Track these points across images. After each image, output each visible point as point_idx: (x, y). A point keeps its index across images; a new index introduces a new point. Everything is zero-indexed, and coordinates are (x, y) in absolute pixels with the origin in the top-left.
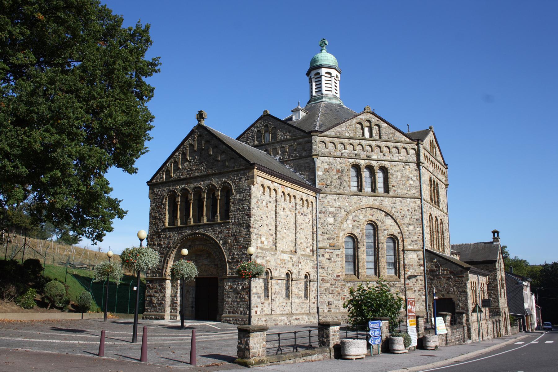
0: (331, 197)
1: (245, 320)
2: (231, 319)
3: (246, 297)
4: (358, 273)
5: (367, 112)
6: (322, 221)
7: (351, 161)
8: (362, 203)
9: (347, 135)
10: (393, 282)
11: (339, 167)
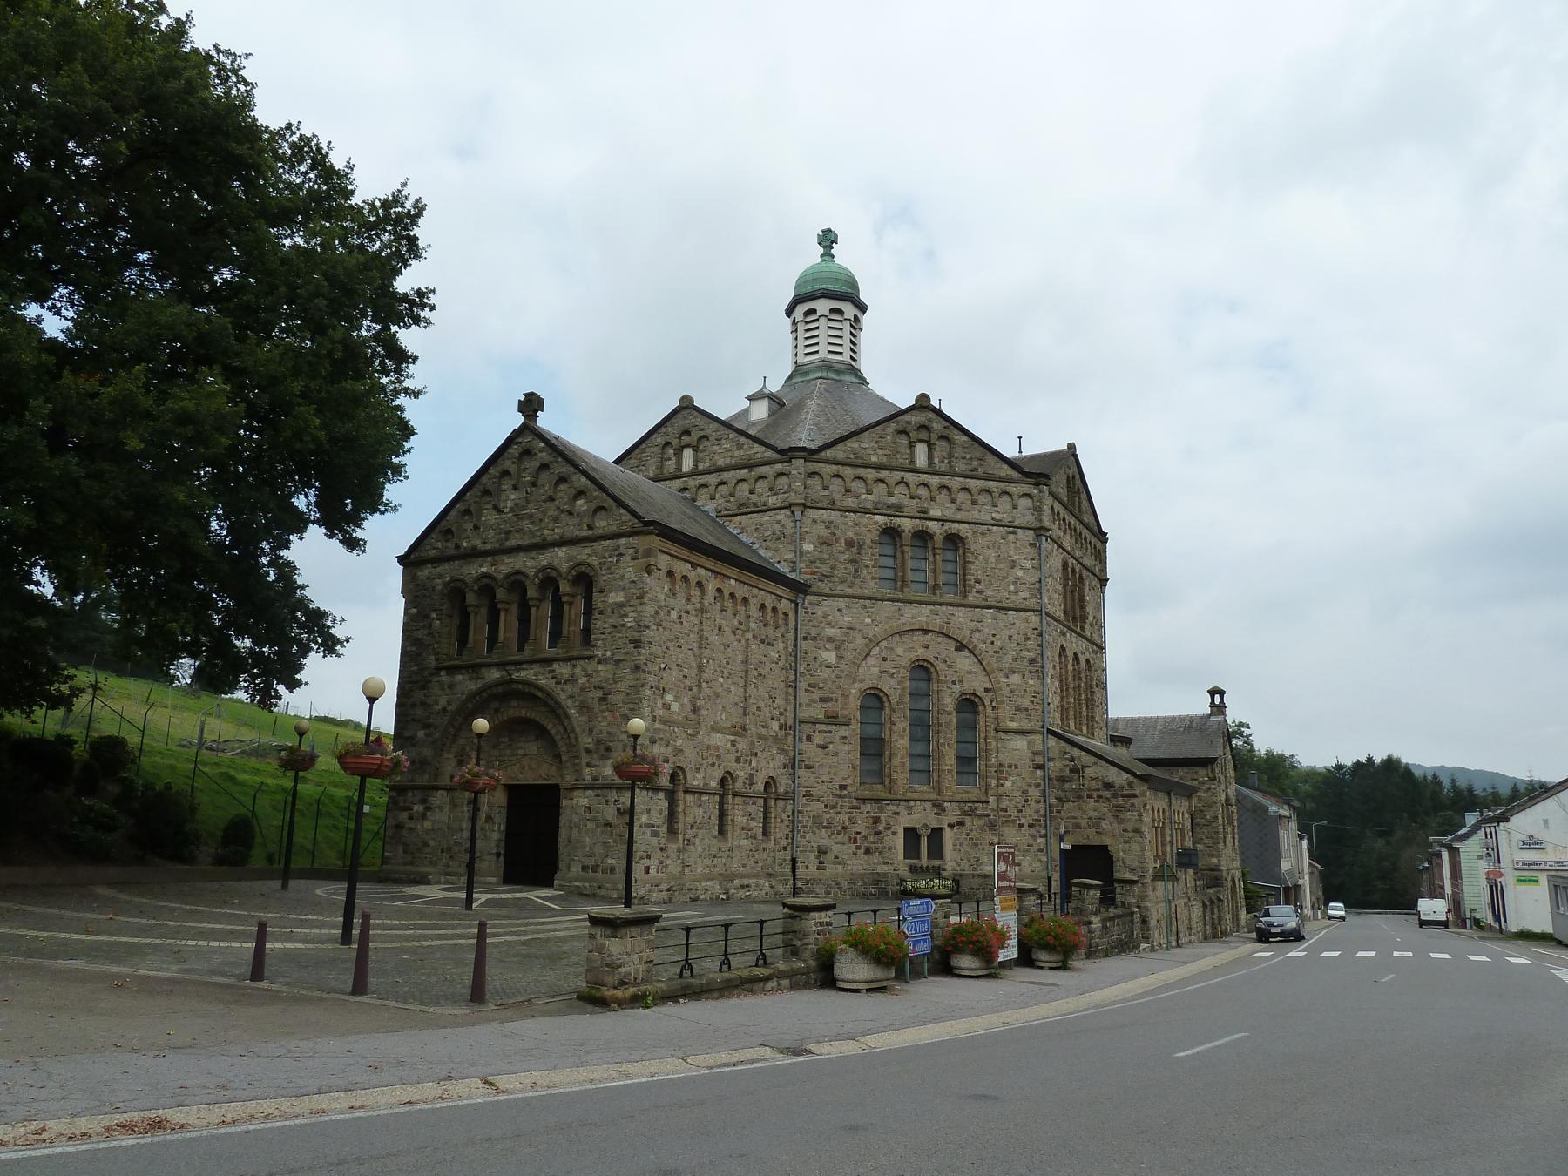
8: (903, 620)
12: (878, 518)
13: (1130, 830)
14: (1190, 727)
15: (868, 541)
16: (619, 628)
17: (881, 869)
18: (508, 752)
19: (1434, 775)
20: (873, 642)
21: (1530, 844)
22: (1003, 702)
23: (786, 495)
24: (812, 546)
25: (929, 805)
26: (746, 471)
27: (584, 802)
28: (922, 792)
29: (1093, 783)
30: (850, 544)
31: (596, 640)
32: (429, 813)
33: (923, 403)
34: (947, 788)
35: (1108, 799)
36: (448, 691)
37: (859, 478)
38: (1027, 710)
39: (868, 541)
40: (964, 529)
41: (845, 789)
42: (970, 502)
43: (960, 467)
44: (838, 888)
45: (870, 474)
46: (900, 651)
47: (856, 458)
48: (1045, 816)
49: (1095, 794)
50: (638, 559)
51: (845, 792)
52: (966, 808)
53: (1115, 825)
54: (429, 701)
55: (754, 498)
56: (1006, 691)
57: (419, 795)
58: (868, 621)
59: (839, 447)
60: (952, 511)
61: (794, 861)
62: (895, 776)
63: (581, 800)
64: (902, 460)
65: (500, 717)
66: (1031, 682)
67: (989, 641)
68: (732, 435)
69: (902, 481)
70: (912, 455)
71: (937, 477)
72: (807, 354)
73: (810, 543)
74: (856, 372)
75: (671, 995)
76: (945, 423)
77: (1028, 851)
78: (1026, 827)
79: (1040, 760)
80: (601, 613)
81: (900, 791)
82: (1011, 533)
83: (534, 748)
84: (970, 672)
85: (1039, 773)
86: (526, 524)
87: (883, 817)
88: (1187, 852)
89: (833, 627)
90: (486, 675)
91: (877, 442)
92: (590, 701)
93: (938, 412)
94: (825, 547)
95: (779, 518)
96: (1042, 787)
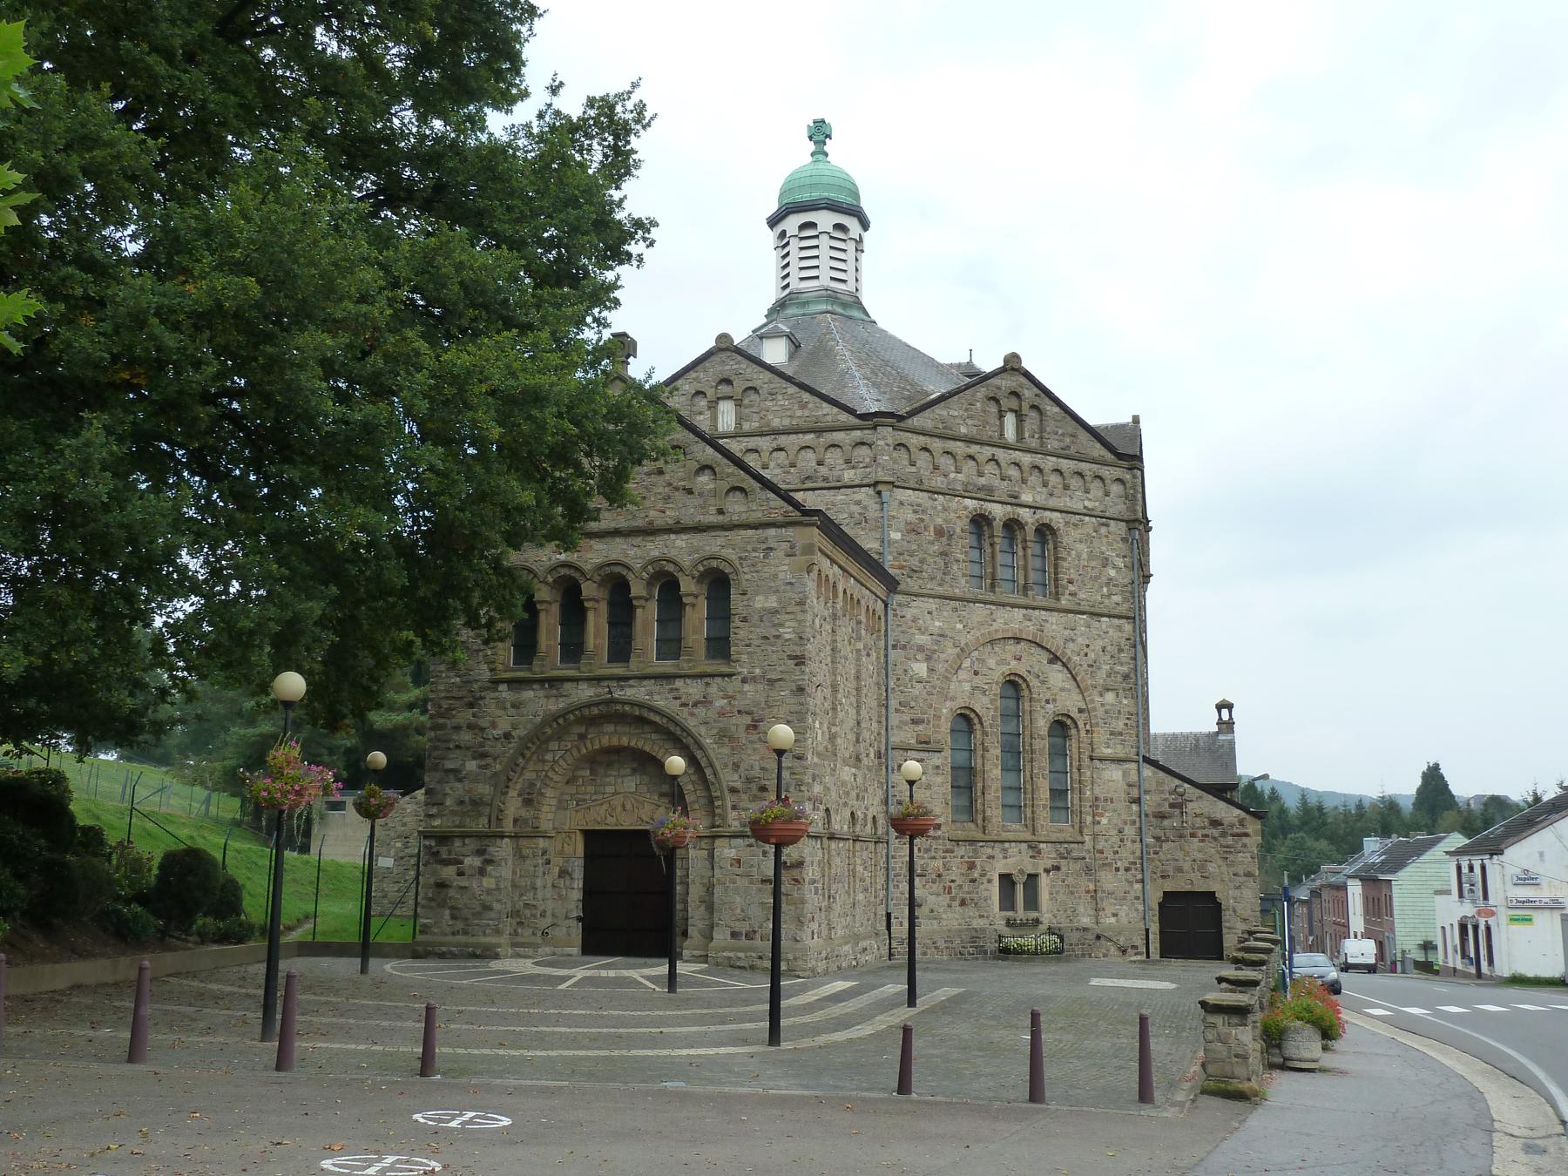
8: (995, 626)
12: (968, 502)
13: (1241, 873)
14: (1197, 746)
15: (958, 530)
16: (772, 640)
17: (978, 923)
18: (591, 789)
19: (1273, 789)
20: (964, 652)
21: (1525, 879)
22: (1097, 725)
23: (868, 470)
24: (899, 534)
25: (1024, 846)
26: (812, 436)
27: (732, 853)
28: (1015, 831)
29: (1198, 819)
30: (940, 532)
31: (739, 653)
32: (489, 868)
33: (1013, 365)
34: (1042, 825)
35: (1215, 839)
36: (512, 711)
37: (948, 453)
38: (1121, 734)
39: (958, 530)
40: (1055, 518)
41: (939, 829)
42: (1061, 486)
43: (1052, 444)
44: (936, 948)
45: (959, 448)
46: (992, 662)
47: (944, 428)
48: (1142, 858)
49: (1200, 833)
50: (795, 555)
51: (939, 833)
52: (1062, 850)
53: (1224, 868)
54: (483, 723)
55: (823, 470)
56: (1100, 712)
57: (472, 845)
58: (959, 626)
59: (927, 413)
60: (1044, 497)
61: (889, 916)
62: (988, 813)
63: (726, 851)
64: (991, 432)
65: (589, 745)
66: (1125, 702)
67: (1082, 654)
68: (792, 389)
69: (993, 459)
70: (1002, 426)
71: (1029, 455)
72: (802, 279)
73: (898, 530)
74: (858, 304)
76: (1036, 390)
77: (1125, 898)
78: (1122, 871)
79: (1135, 793)
80: (745, 620)
81: (994, 831)
82: (1103, 524)
83: (630, 783)
84: (1062, 689)
85: (1135, 807)
87: (978, 862)
88: (1271, 897)
89: (923, 634)
90: (573, 692)
91: (966, 410)
92: (733, 729)
93: (1027, 375)
94: (913, 536)
95: (857, 497)
96: (1138, 825)
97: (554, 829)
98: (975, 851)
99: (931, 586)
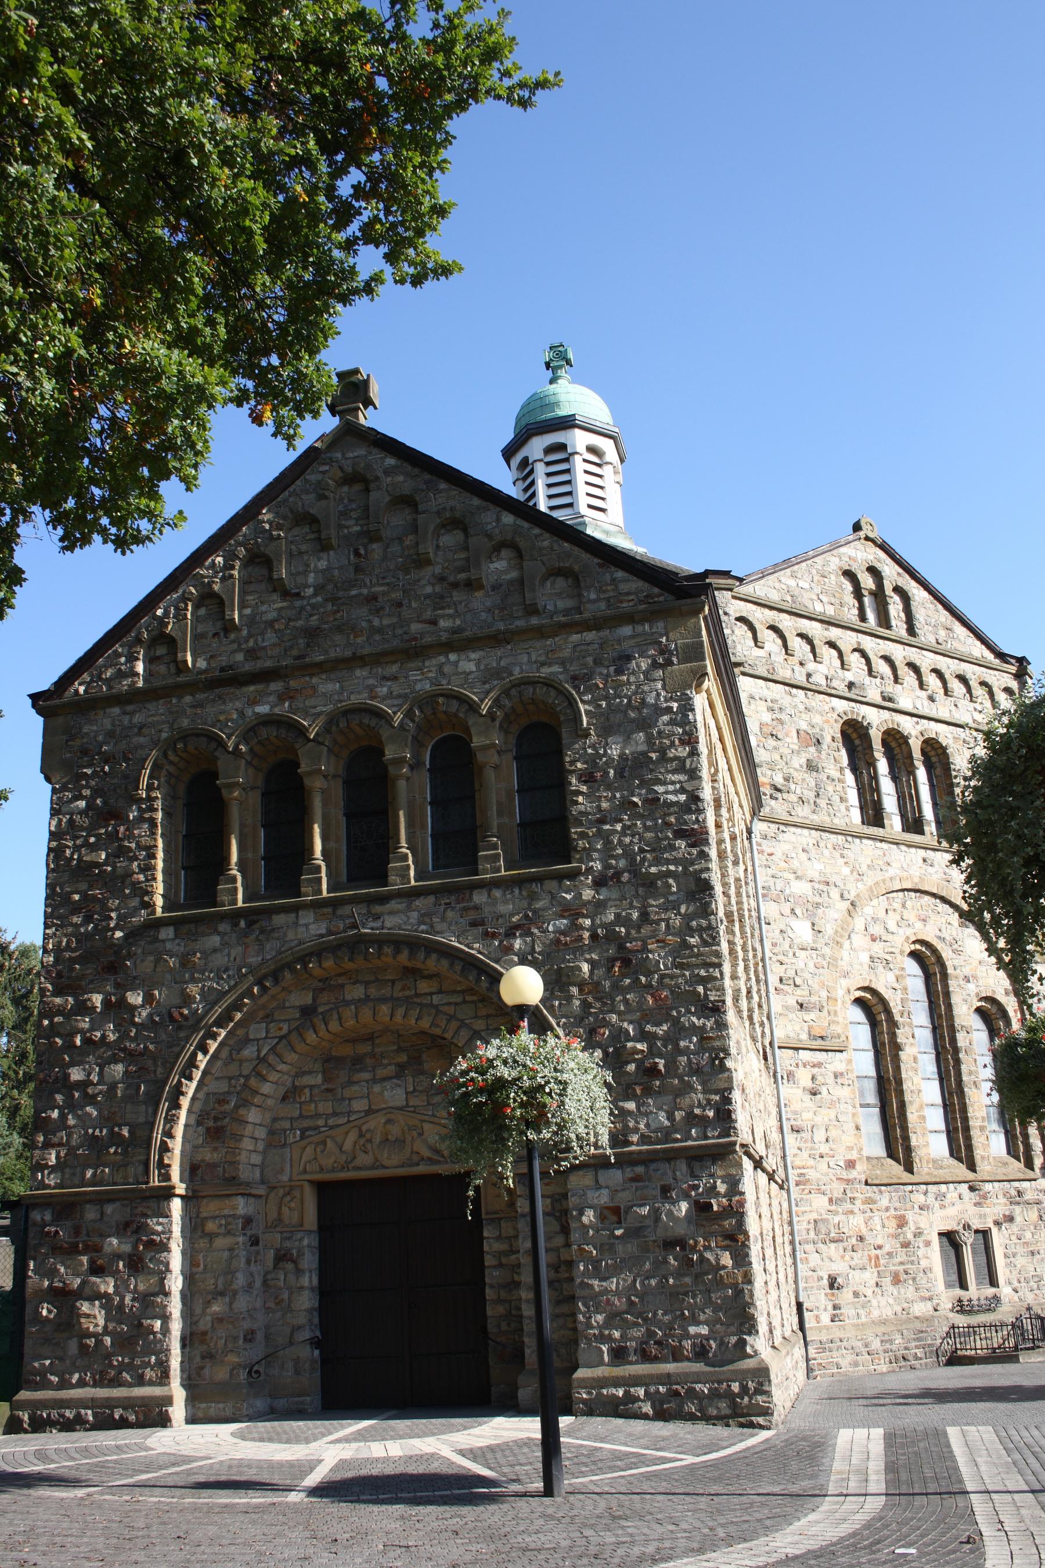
0: (793, 838)
1: (735, 1387)
2: (641, 1392)
3: (727, 1260)
4: (908, 1149)
5: (867, 538)
6: (776, 927)
7: (841, 705)
8: (892, 872)
9: (819, 608)
10: (1016, 1184)
11: (804, 726)
17: (921, 1309)
61: (799, 1306)
75: (265, 1477)
86: (361, 614)
97: (263, 1182)
98: (902, 1199)
99: (803, 813)
